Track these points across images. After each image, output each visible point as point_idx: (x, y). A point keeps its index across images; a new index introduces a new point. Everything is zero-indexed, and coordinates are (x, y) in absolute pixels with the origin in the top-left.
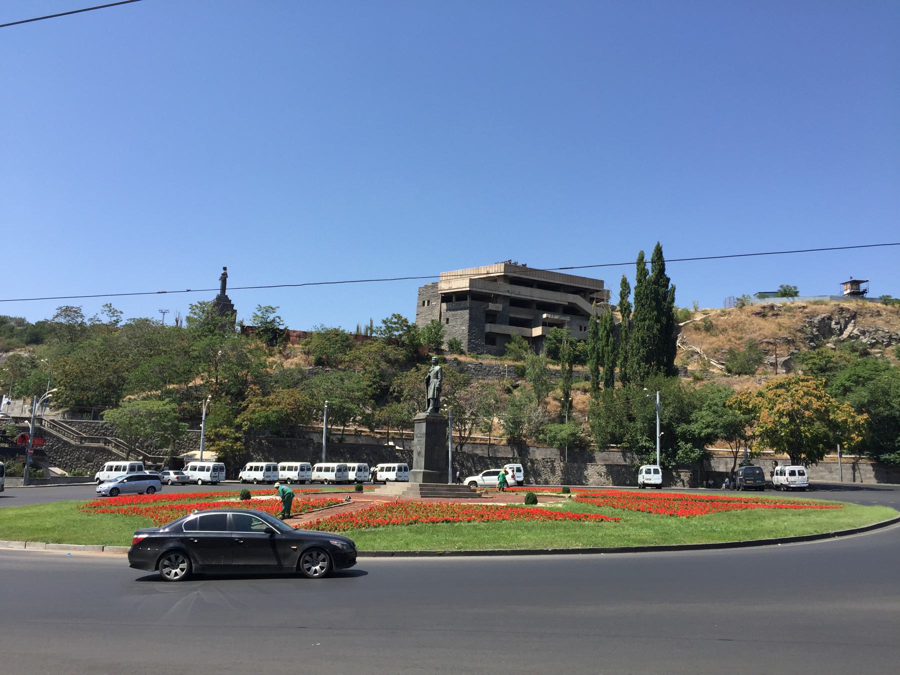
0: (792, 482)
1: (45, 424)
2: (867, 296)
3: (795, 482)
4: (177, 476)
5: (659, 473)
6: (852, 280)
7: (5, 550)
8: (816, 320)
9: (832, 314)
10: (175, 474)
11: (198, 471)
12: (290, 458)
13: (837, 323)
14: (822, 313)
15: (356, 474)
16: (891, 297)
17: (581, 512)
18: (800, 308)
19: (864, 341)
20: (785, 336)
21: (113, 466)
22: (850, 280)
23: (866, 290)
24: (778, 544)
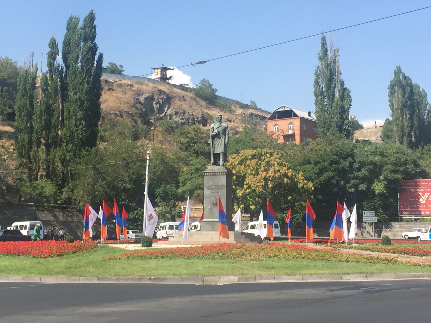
0: (170, 234)
1: (375, 200)
2: (170, 81)
3: (173, 234)
4: (135, 234)
5: (278, 228)
6: (164, 67)
7: (392, 280)
8: (142, 99)
9: (153, 94)
10: (133, 232)
11: (251, 229)
12: (26, 217)
13: (157, 103)
14: (146, 93)
15: (28, 232)
16: (389, 105)
17: (178, 261)
18: (128, 86)
19: (177, 120)
20: (126, 110)
21: (18, 226)
22: (162, 67)
23: (171, 77)
24: (214, 285)
